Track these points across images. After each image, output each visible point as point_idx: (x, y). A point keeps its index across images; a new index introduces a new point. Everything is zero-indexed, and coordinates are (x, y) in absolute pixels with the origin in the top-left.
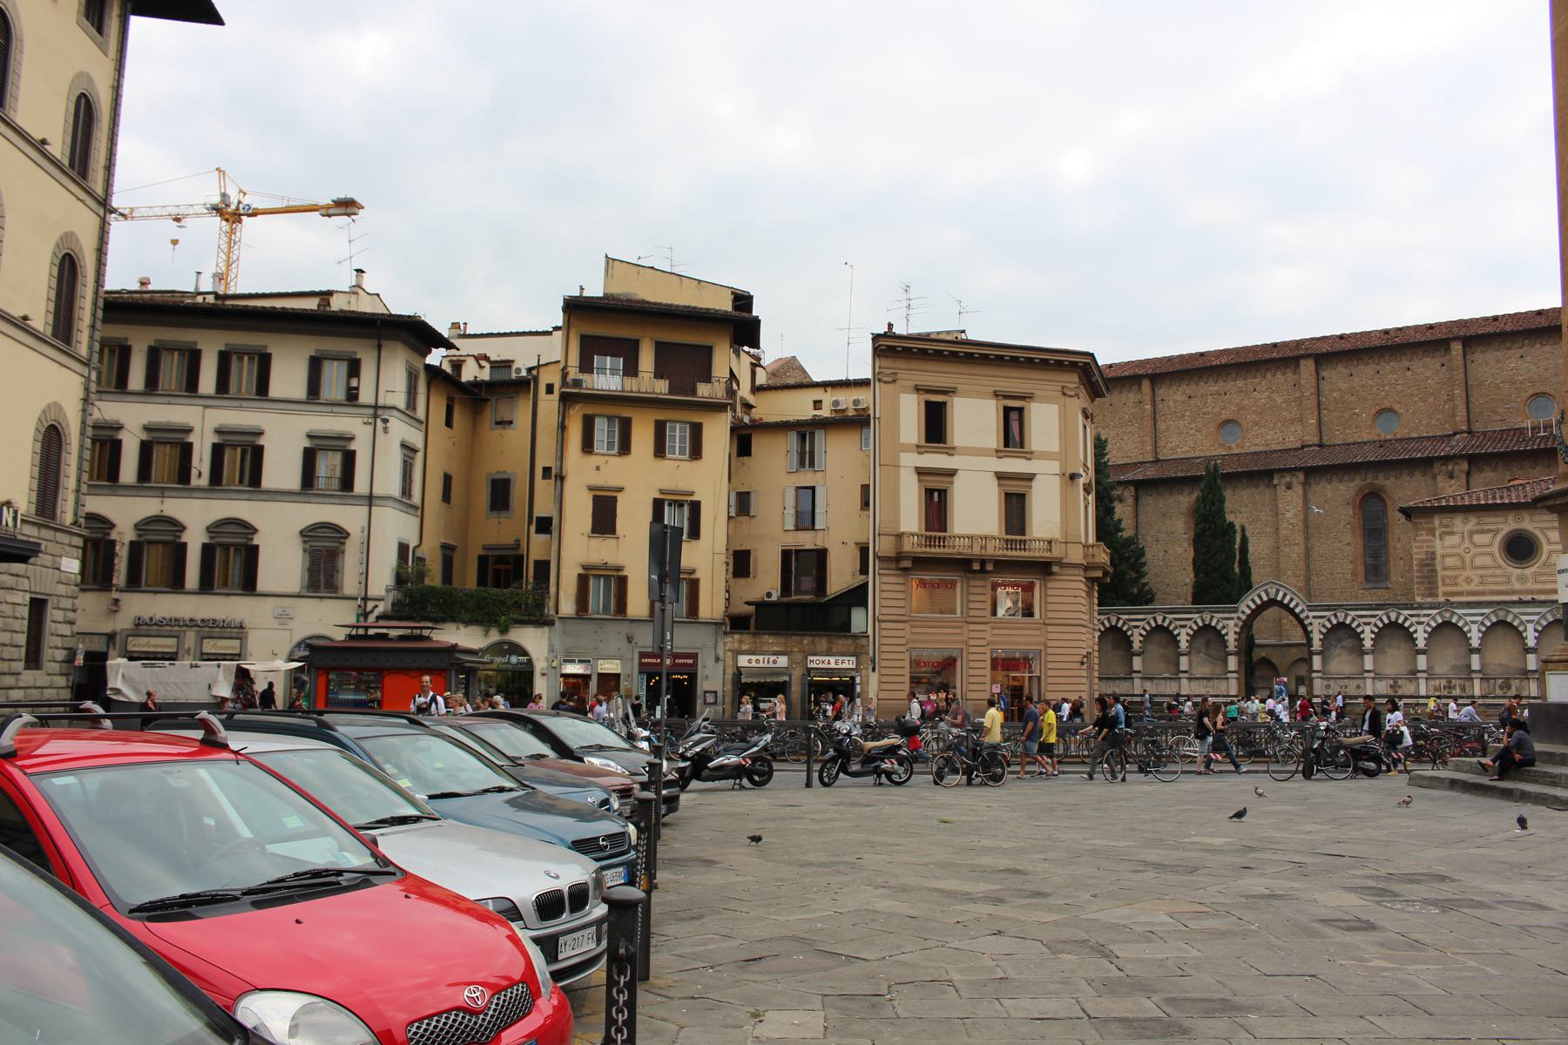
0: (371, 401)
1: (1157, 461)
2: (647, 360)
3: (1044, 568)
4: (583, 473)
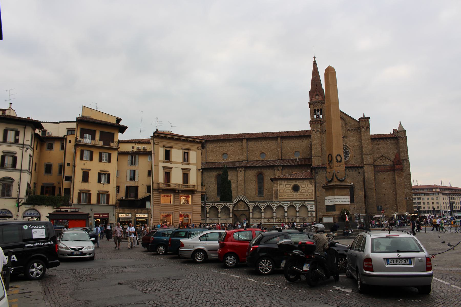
0: (22, 143)
1: (206, 163)
2: (98, 136)
3: (192, 192)
4: (80, 165)
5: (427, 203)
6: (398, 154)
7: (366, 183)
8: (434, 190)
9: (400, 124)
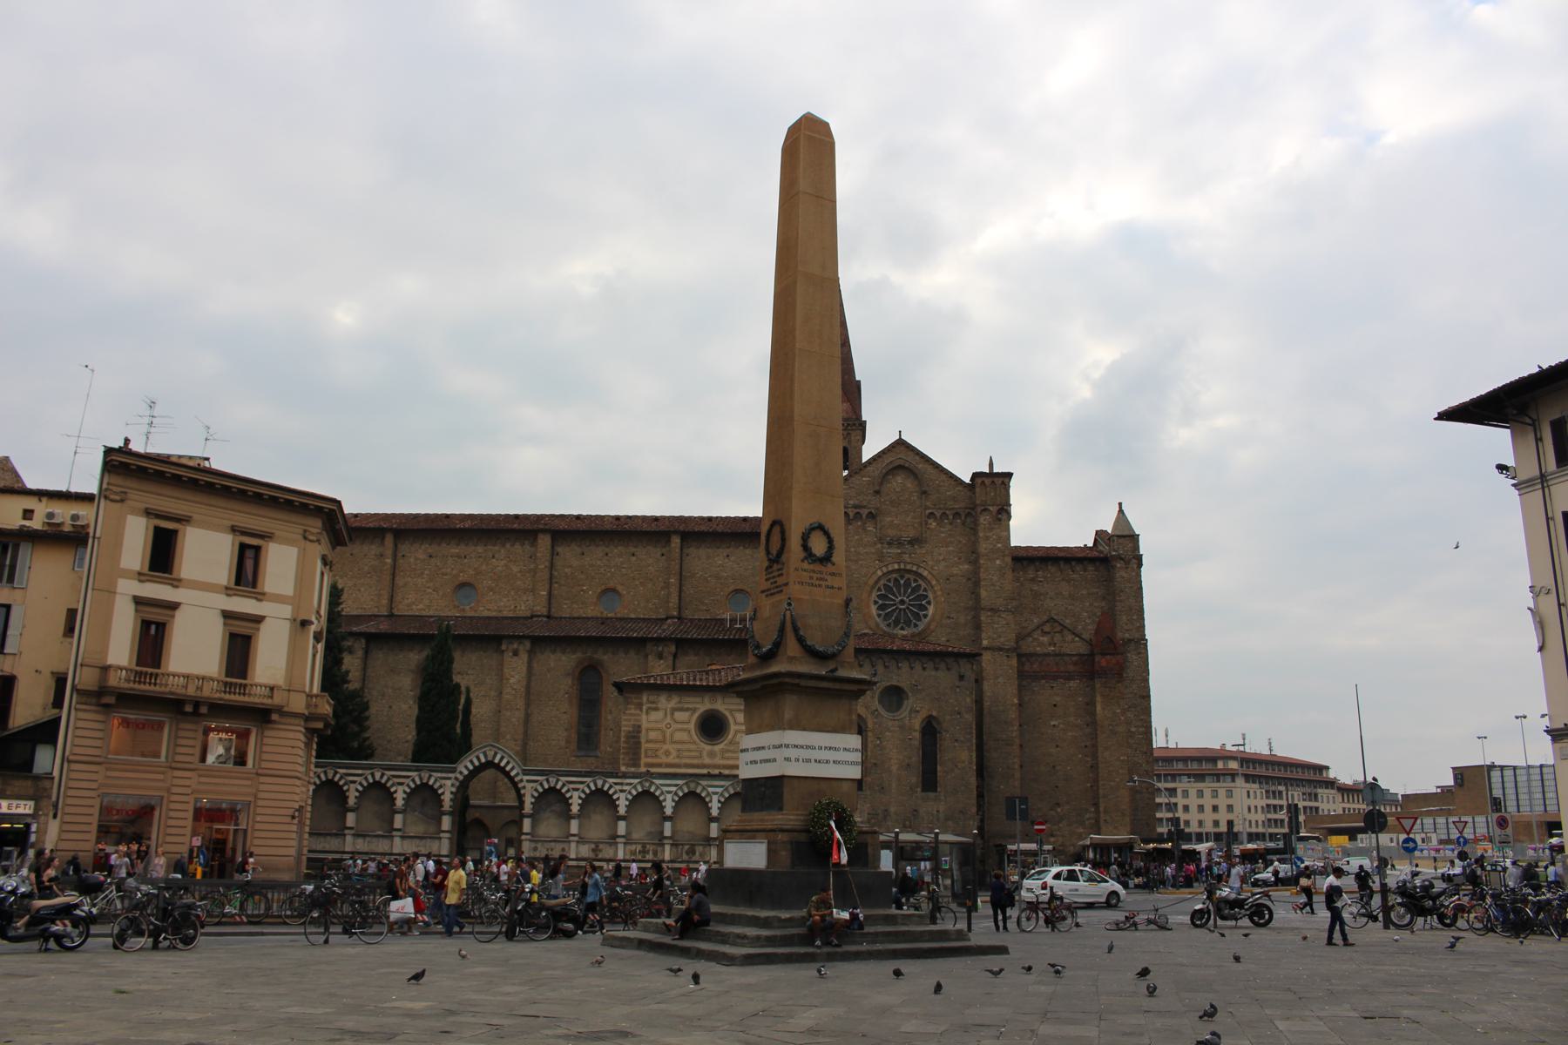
1: (391, 615)
3: (263, 715)
5: (1198, 808)
6: (1107, 623)
7: (987, 720)
8: (1220, 765)
9: (1121, 511)
